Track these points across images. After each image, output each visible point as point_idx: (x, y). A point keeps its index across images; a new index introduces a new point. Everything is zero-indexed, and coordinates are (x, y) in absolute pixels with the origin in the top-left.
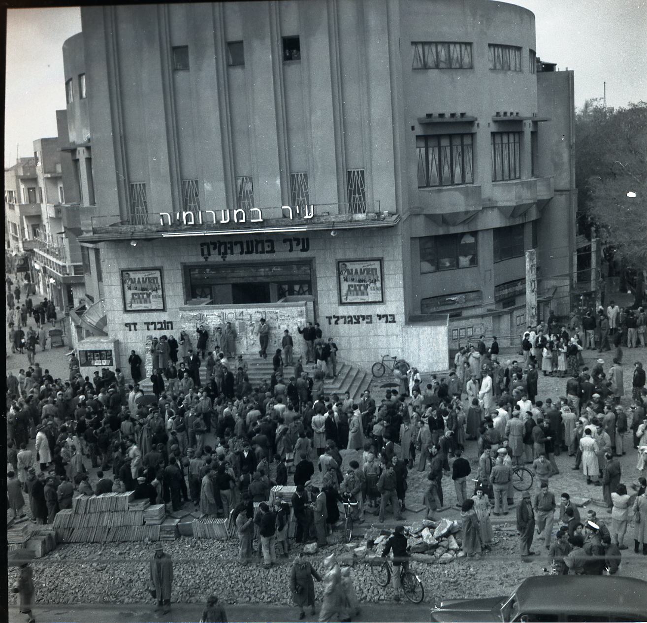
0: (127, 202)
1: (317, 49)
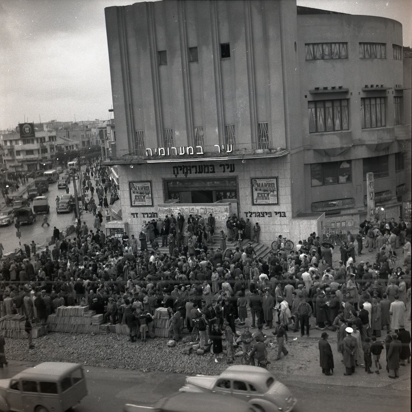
0: (133, 141)
1: (239, 51)
